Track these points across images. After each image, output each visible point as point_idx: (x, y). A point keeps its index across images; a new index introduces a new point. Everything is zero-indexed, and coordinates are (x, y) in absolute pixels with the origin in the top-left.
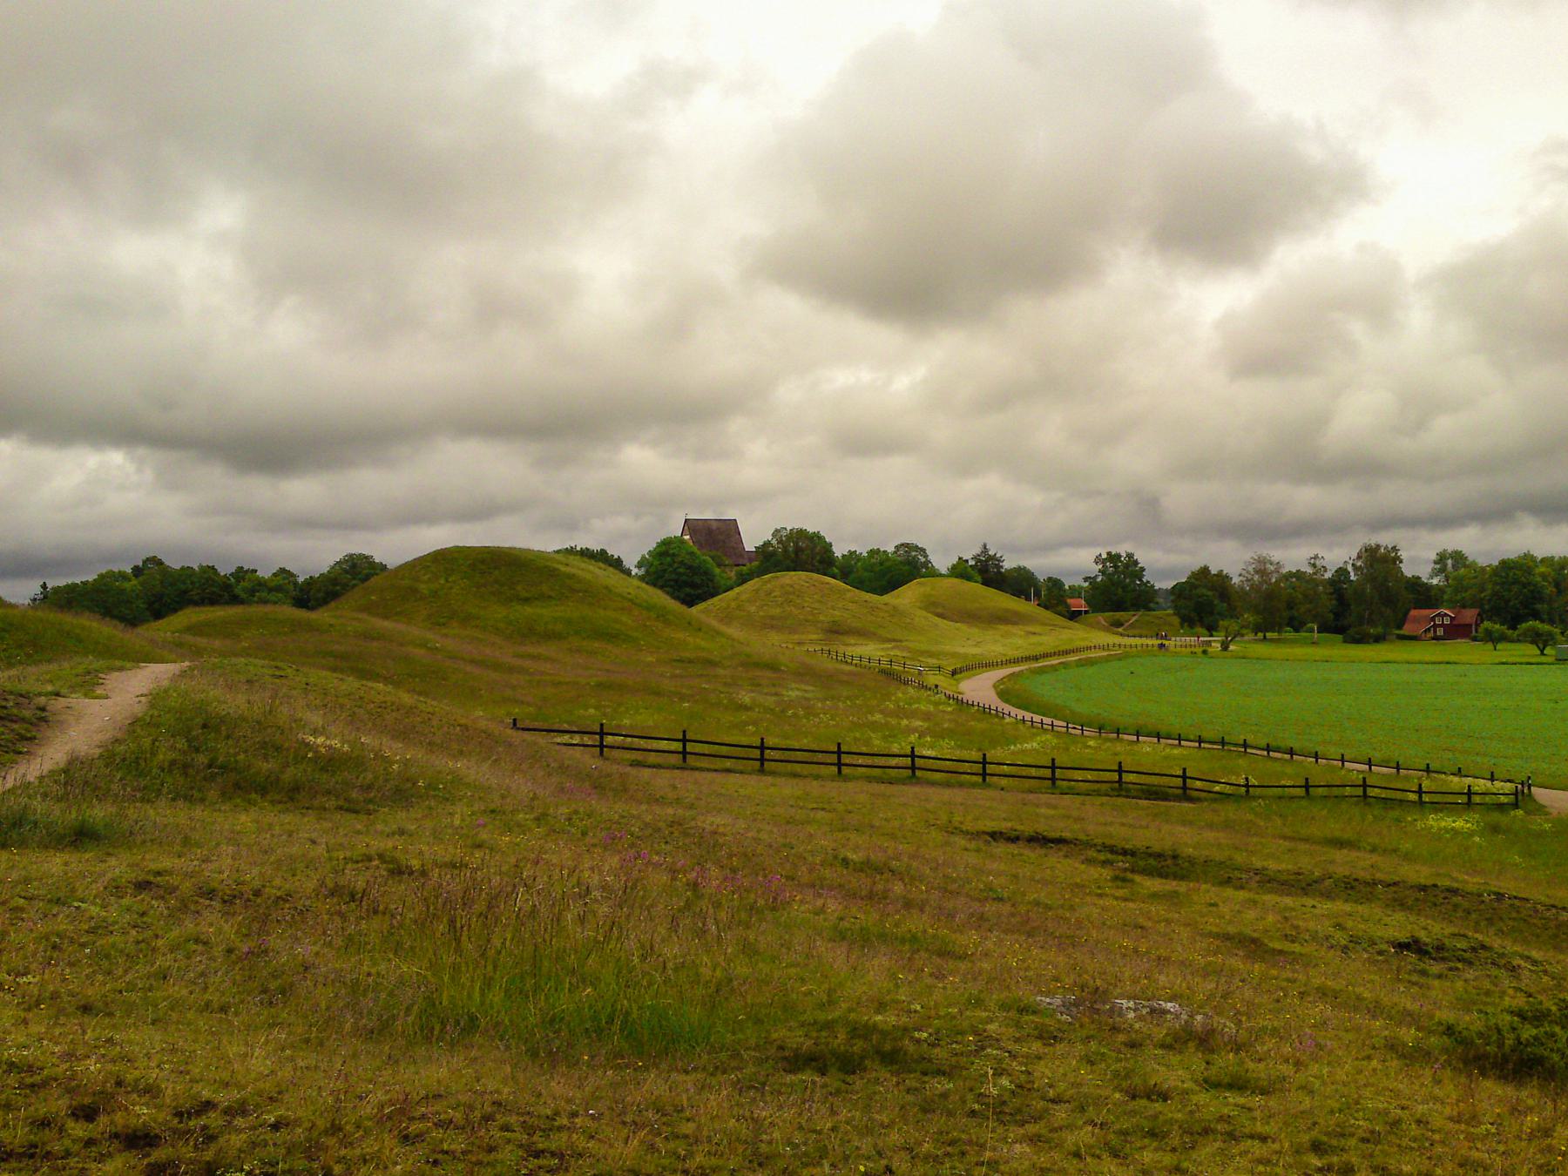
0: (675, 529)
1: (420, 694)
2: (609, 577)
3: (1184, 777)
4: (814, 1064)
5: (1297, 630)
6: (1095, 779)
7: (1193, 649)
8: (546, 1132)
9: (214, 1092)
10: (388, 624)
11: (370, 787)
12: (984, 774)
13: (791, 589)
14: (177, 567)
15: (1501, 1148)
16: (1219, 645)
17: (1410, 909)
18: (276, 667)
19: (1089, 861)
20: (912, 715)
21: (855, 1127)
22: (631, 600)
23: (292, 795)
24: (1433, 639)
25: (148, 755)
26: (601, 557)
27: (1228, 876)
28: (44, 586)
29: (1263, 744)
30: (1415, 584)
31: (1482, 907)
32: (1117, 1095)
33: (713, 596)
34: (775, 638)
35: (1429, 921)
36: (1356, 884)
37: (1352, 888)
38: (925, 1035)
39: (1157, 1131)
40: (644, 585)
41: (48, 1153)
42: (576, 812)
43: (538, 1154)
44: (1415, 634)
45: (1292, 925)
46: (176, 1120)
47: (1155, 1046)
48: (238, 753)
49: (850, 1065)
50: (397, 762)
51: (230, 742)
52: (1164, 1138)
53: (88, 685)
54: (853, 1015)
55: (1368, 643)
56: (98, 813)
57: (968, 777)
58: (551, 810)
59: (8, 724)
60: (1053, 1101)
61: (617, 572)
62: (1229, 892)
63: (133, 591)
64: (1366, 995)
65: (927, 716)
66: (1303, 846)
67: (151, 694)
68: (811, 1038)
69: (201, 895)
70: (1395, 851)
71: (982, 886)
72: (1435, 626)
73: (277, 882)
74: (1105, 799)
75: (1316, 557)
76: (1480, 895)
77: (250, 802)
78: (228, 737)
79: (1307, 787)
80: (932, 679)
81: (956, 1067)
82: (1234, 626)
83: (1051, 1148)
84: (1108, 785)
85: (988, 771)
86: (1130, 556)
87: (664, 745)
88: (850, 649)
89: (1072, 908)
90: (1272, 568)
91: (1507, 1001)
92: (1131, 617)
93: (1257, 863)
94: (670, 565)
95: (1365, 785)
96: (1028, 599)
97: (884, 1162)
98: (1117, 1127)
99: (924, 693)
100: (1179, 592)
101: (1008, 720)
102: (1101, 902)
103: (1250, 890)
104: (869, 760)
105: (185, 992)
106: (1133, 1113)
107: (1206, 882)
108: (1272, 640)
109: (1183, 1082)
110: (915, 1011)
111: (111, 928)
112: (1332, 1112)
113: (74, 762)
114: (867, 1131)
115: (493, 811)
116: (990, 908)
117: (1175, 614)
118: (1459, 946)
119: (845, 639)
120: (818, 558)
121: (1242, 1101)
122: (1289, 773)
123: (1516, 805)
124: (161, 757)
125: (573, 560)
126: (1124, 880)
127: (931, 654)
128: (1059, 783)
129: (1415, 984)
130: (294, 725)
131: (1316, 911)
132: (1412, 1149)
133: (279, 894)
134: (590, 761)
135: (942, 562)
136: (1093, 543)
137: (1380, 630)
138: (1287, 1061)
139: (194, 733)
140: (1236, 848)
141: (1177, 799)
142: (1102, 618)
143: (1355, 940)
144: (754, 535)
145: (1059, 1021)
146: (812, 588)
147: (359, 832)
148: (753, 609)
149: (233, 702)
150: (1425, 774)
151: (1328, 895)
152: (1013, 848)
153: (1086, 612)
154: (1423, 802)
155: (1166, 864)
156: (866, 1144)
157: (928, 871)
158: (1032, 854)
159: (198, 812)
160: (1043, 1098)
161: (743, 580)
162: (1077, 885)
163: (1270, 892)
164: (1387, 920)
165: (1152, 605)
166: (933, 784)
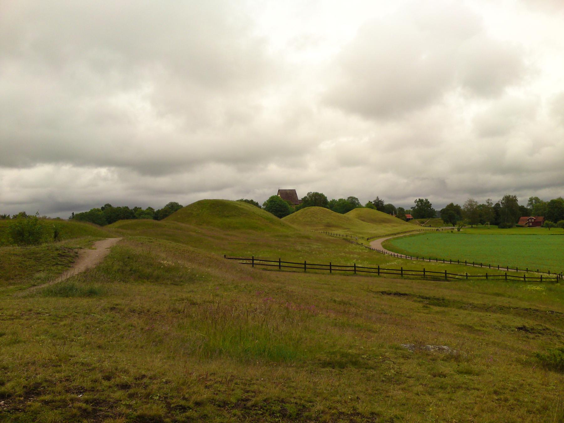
0: (275, 193)
1: (195, 247)
2: (255, 209)
3: (446, 273)
4: (330, 365)
5: (483, 224)
6: (416, 274)
7: (448, 231)
8: (249, 385)
9: (145, 372)
10: (183, 225)
11: (181, 277)
12: (379, 273)
13: (313, 212)
14: (346, 199)
15: (557, 394)
16: (457, 229)
17: (522, 316)
18: (150, 239)
19: (415, 301)
20: (353, 253)
21: (346, 385)
22: (261, 216)
23: (157, 279)
24: (529, 227)
25: (111, 267)
26: (251, 202)
27: (461, 306)
28: (73, 214)
29: (472, 262)
30: (522, 208)
31: (546, 315)
32: (429, 376)
33: (288, 215)
34: (308, 228)
35: (529, 320)
36: (504, 308)
37: (502, 309)
38: (366, 356)
39: (443, 387)
40: (265, 211)
41: (98, 390)
42: (247, 285)
43: (248, 392)
44: (522, 225)
45: (483, 321)
46: (135, 381)
47: (441, 360)
48: (139, 266)
49: (342, 366)
50: (189, 269)
51: (137, 263)
52: (445, 389)
53: (90, 245)
54: (341, 350)
55: (506, 228)
56: (96, 286)
57: (373, 273)
58: (239, 284)
59: (66, 258)
60: (409, 377)
61: (257, 207)
62: (462, 311)
63: (102, 215)
64: (508, 344)
65: (359, 254)
66: (485, 296)
67: (110, 248)
68: (329, 357)
69: (131, 312)
70: (517, 297)
71: (380, 309)
72: (529, 222)
73: (155, 307)
74: (419, 281)
75: (489, 200)
76: (546, 312)
77: (144, 282)
78: (136, 261)
79: (487, 276)
80: (360, 241)
81: (376, 367)
82: (461, 223)
83: (409, 392)
84: (420, 276)
85: (380, 272)
86: (426, 200)
87: (273, 263)
88: (333, 231)
89: (410, 316)
90: (474, 203)
91: (557, 347)
92: (427, 220)
93: (471, 301)
94: (274, 205)
95: (506, 275)
96: (392, 214)
97: (356, 396)
98: (430, 385)
99: (358, 246)
100: (443, 212)
101: (386, 255)
102: (419, 314)
103: (469, 310)
104: (340, 268)
105: (129, 342)
106: (435, 381)
107: (454, 308)
108: (475, 228)
109: (450, 371)
110: (362, 349)
111: (104, 322)
112: (500, 381)
113: (87, 270)
114: (350, 386)
115: (221, 285)
116: (383, 316)
117: (441, 219)
118: (539, 328)
119: (333, 229)
120: (322, 202)
121: (470, 377)
122: (481, 272)
123: (557, 282)
124: (115, 268)
125: (243, 204)
126: (427, 307)
127: (360, 233)
128: (404, 275)
129: (525, 341)
130: (157, 257)
131: (491, 317)
132: (527, 394)
133: (156, 311)
134: (249, 268)
135: (363, 202)
136: (414, 196)
137: (510, 224)
138: (484, 365)
139: (125, 260)
140: (464, 297)
141: (443, 280)
142: (417, 221)
143: (504, 326)
144: (301, 194)
145: (409, 352)
146: (320, 212)
147: (179, 291)
148: (301, 219)
149: (138, 250)
150: (526, 271)
151: (494, 312)
152: (389, 297)
153: (412, 219)
154: (525, 281)
155: (440, 302)
156: (350, 390)
157: (362, 304)
158: (396, 298)
159: (128, 285)
160: (405, 376)
161: (298, 209)
162: (411, 309)
163: (475, 310)
164: (514, 320)
165: (434, 216)
166: (362, 276)
